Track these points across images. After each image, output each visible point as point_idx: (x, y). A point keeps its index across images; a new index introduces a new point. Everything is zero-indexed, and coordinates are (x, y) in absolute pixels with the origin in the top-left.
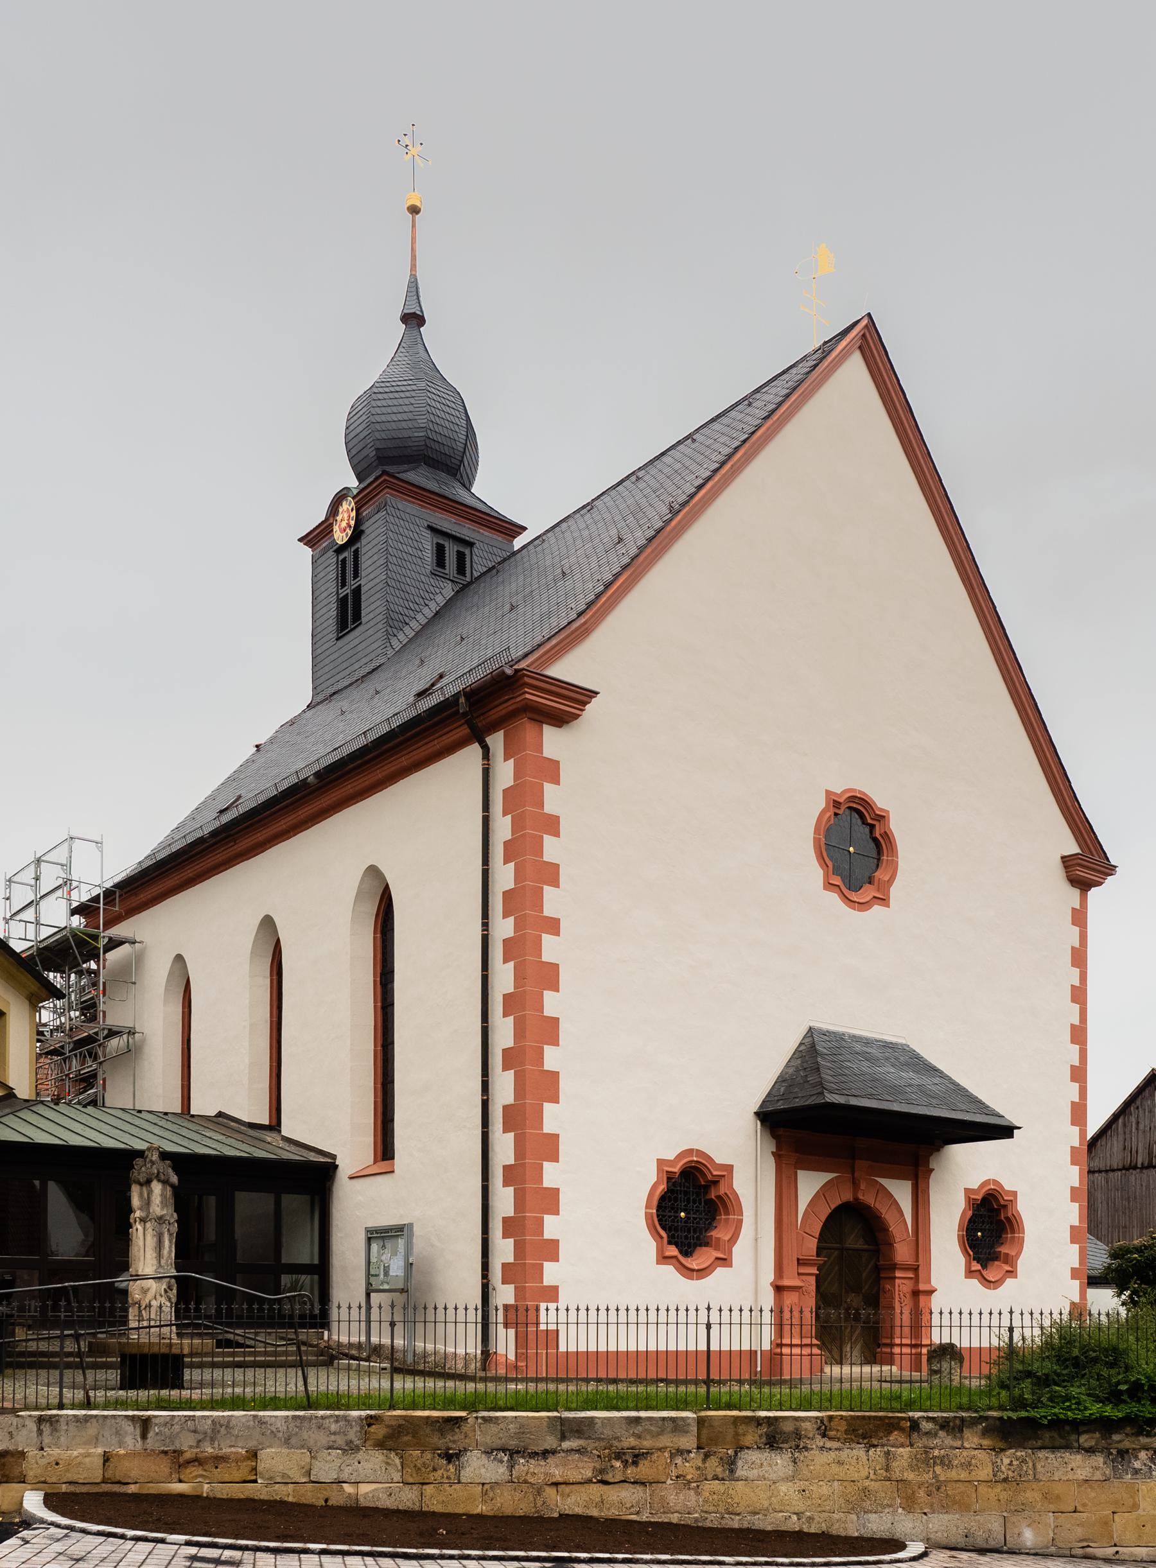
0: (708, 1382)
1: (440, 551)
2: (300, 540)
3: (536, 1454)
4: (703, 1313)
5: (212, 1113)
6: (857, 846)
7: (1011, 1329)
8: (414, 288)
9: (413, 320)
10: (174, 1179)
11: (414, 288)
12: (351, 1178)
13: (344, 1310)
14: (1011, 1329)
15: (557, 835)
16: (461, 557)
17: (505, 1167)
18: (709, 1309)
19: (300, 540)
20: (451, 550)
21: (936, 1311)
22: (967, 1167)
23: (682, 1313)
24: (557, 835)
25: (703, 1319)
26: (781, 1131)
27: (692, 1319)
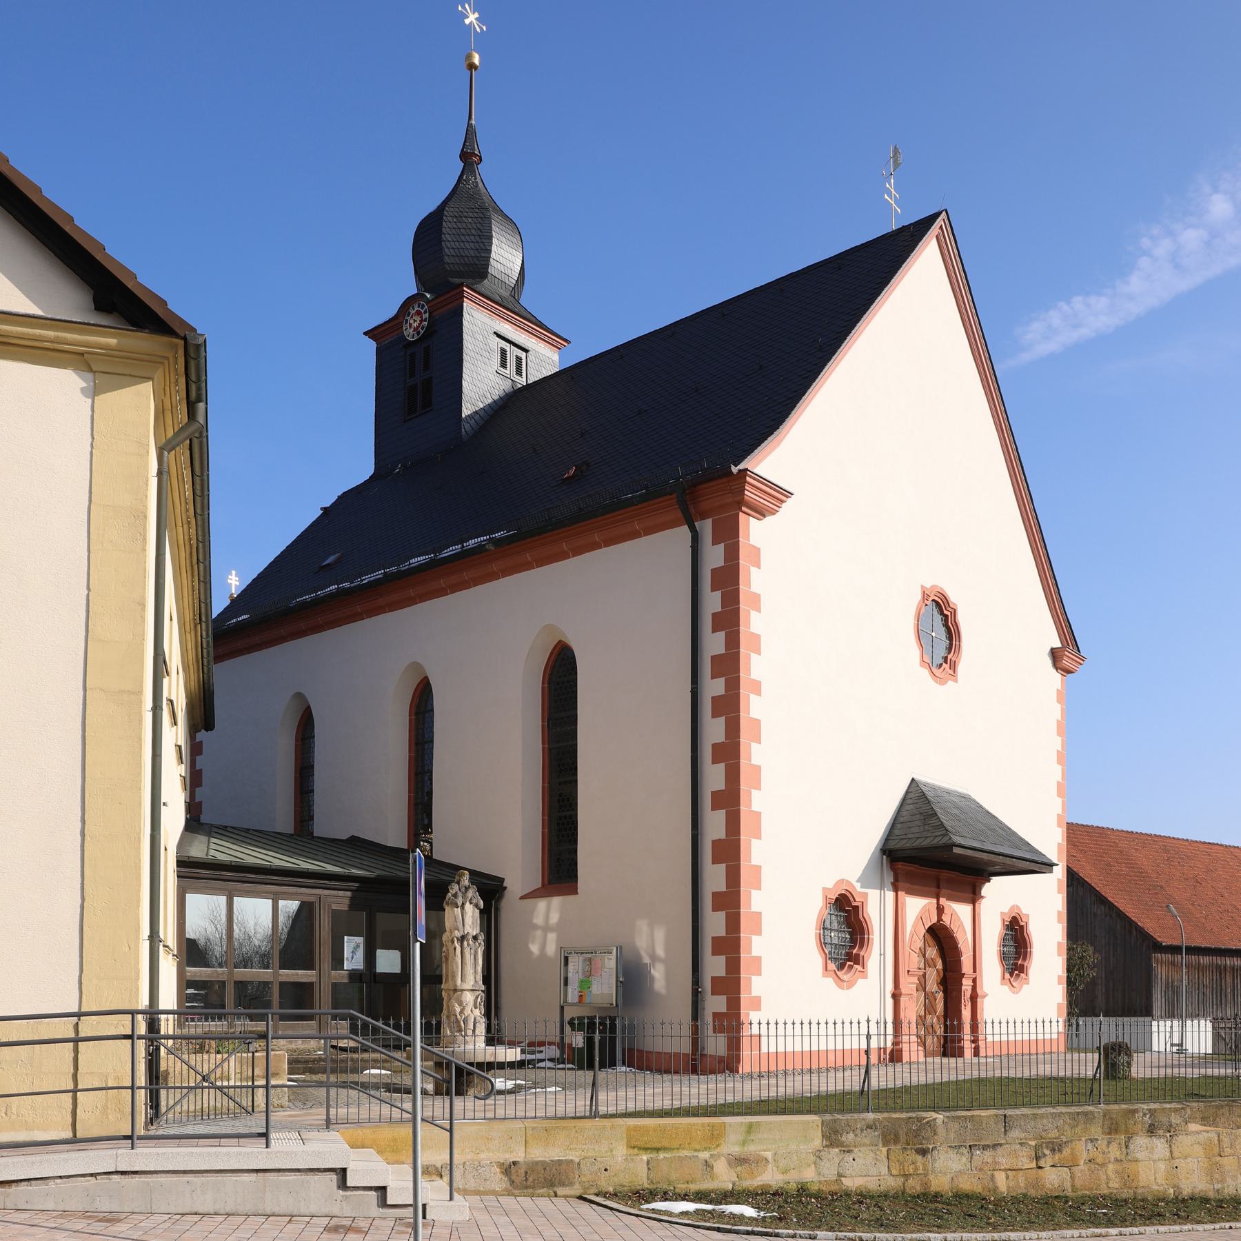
0: (267, 1087)
1: (503, 352)
2: (365, 333)
3: (988, 1146)
4: (864, 1025)
5: (344, 836)
6: (942, 625)
7: (868, 1037)
8: (470, 134)
9: (469, 157)
10: (481, 904)
11: (470, 134)
12: (522, 898)
13: (989, 1026)
14: (868, 1037)
15: (759, 611)
16: (519, 359)
17: (714, 894)
18: (868, 1021)
19: (365, 333)
20: (512, 352)
21: (989, 1021)
22: (1001, 895)
23: (831, 1026)
24: (759, 611)
25: (864, 1031)
26: (900, 865)
27: (855, 1031)
